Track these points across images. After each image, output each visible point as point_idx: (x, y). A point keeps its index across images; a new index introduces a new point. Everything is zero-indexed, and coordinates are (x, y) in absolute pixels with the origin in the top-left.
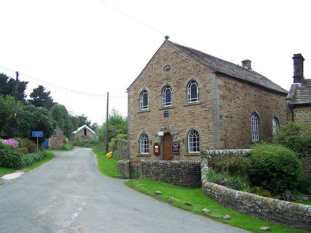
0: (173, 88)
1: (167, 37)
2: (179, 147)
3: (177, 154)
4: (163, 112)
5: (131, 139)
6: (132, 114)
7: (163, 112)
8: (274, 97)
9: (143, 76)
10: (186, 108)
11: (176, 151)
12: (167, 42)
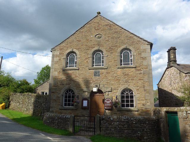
5: (53, 93)
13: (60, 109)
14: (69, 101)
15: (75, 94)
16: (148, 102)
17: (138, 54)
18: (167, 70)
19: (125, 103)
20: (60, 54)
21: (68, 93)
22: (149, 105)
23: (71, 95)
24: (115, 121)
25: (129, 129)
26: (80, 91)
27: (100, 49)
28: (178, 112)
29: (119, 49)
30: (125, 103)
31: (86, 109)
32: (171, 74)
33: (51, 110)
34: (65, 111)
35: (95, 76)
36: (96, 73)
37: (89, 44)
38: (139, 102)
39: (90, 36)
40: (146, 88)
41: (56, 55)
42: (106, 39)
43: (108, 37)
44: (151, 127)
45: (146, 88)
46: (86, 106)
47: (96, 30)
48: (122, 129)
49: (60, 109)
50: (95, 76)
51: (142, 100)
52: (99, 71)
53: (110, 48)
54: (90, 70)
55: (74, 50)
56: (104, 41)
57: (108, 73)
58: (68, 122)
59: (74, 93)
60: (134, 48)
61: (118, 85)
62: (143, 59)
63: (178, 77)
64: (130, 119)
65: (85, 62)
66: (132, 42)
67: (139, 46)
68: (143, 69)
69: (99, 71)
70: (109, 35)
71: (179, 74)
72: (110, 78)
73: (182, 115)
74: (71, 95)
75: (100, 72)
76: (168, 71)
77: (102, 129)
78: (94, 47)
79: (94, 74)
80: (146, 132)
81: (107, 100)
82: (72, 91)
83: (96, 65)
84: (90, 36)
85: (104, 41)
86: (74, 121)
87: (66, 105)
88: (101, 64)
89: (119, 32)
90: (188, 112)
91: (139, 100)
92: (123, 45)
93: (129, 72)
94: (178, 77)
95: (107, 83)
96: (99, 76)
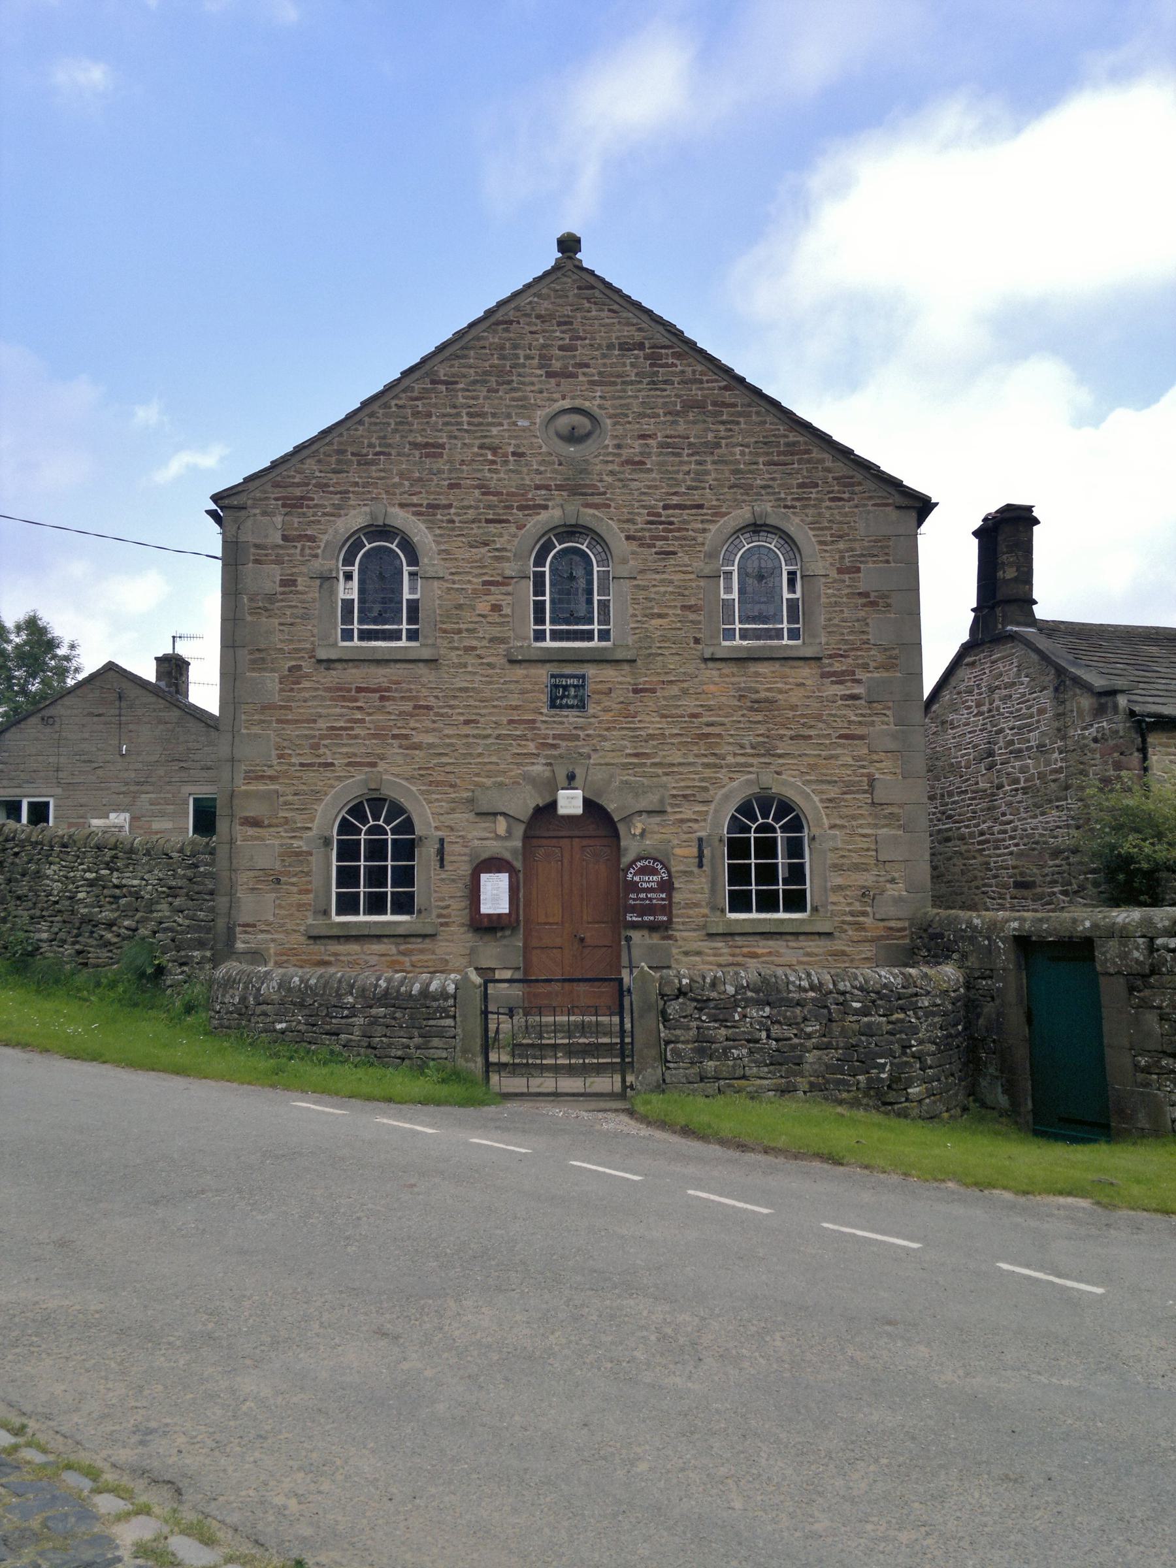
0: (619, 544)
1: (569, 245)
2: (667, 886)
3: (653, 928)
4: (542, 674)
5: (255, 823)
6: (259, 664)
7: (542, 674)
8: (634, 1006)
9: (523, 301)
10: (711, 673)
11: (650, 909)
12: (157, 659)
13: (315, 933)
14: (377, 877)
15: (419, 829)
16: (892, 881)
17: (840, 571)
18: (968, 660)
19: (389, 863)
20: (285, 538)
21: (364, 821)
22: (900, 899)
23: (390, 837)
24: (749, 1002)
25: (827, 1047)
26: (453, 811)
27: (588, 516)
28: (1098, 942)
29: (713, 528)
30: (753, 887)
31: (503, 929)
32: (992, 690)
33: (240, 946)
34: (354, 947)
35: (553, 706)
36: (565, 688)
37: (503, 479)
38: (839, 881)
39: (509, 416)
40: (880, 795)
41: (257, 546)
42: (626, 453)
43: (643, 437)
44: (941, 1028)
45: (880, 795)
46: (507, 911)
47: (549, 375)
48: (794, 1047)
49: (315, 938)
50: (553, 706)
51: (857, 868)
52: (583, 677)
53: (654, 519)
54: (519, 672)
55: (400, 518)
56: (610, 467)
57: (642, 690)
58: (450, 1022)
59: (408, 826)
60: (815, 525)
61: (708, 773)
62: (873, 604)
63: (1041, 711)
64: (835, 984)
65: (483, 607)
66: (800, 486)
67: (846, 515)
68: (865, 666)
69: (583, 677)
70: (648, 426)
71: (1049, 693)
72: (652, 723)
73: (1124, 956)
74: (390, 837)
75: (590, 687)
76: (973, 664)
77: (675, 1051)
78: (546, 507)
79: (545, 698)
80: (918, 1057)
81: (643, 871)
82: (397, 810)
83: (556, 636)
84: (509, 416)
85: (610, 467)
86: (485, 1013)
87: (348, 904)
88: (596, 627)
89: (715, 404)
90: (1159, 941)
91: (837, 868)
92: (738, 504)
93: (780, 691)
94: (1041, 711)
95: (636, 755)
96: (581, 706)
